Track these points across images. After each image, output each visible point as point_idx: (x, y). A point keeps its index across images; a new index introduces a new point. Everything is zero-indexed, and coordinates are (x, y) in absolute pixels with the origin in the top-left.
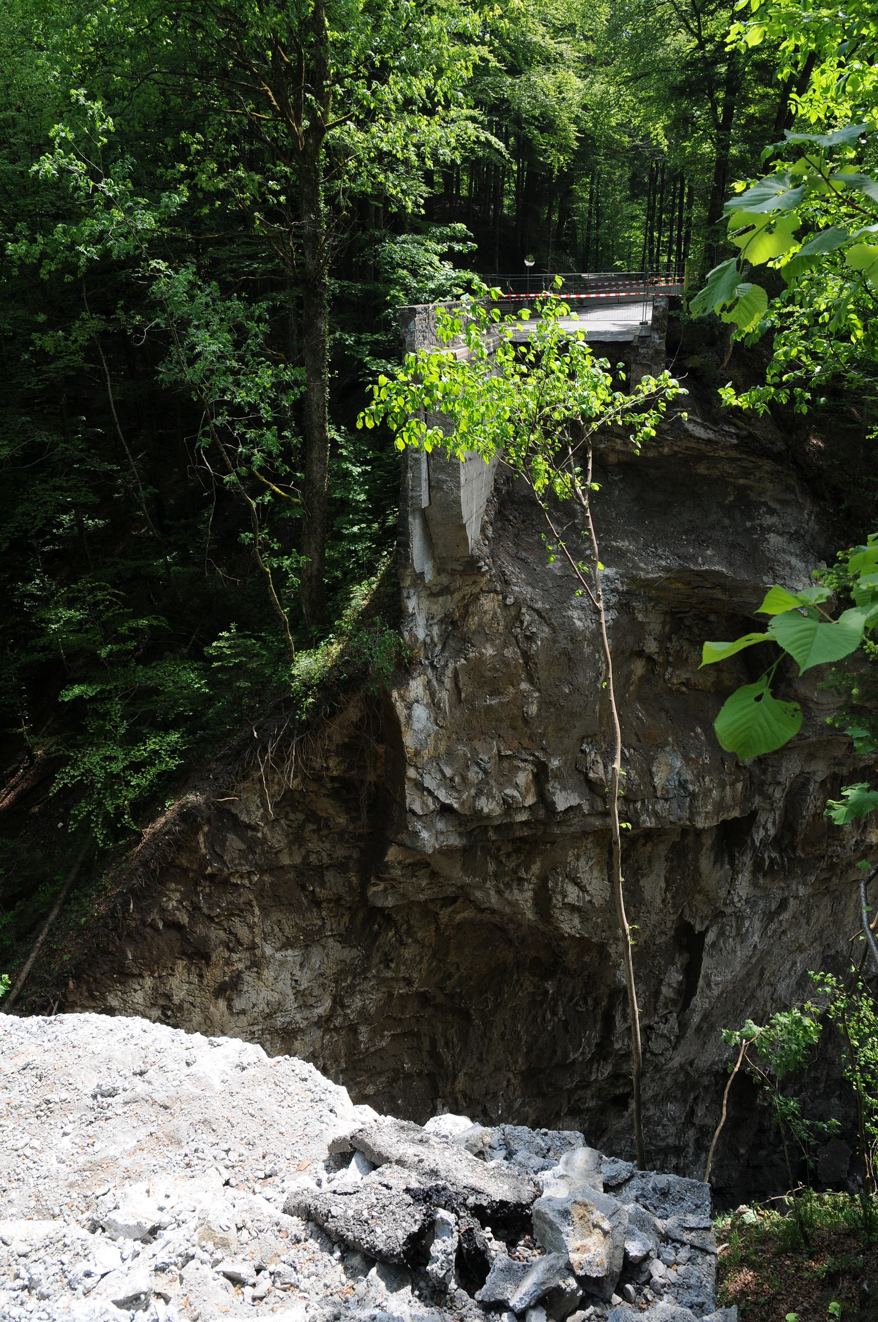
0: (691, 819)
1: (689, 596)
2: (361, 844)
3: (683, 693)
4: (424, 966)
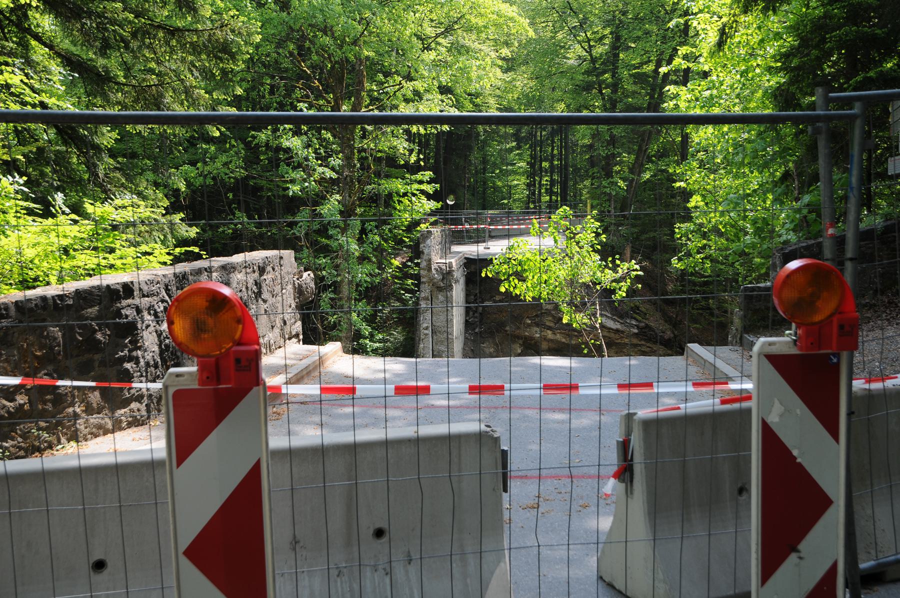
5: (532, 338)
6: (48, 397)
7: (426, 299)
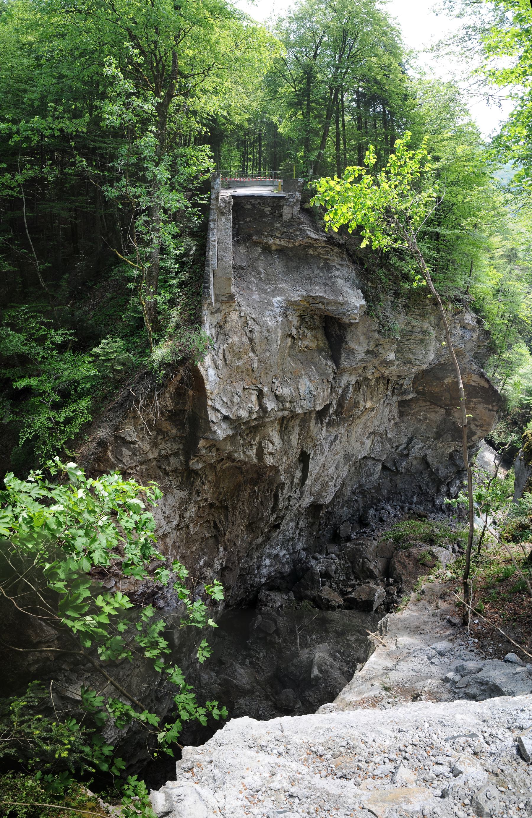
0: (314, 407)
1: (308, 308)
2: (183, 441)
3: (305, 351)
4: (211, 491)
5: (267, 244)
7: (213, 220)
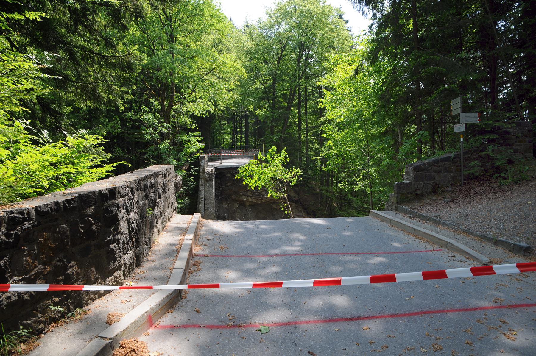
5: (242, 201)
6: (61, 278)
7: (202, 185)
